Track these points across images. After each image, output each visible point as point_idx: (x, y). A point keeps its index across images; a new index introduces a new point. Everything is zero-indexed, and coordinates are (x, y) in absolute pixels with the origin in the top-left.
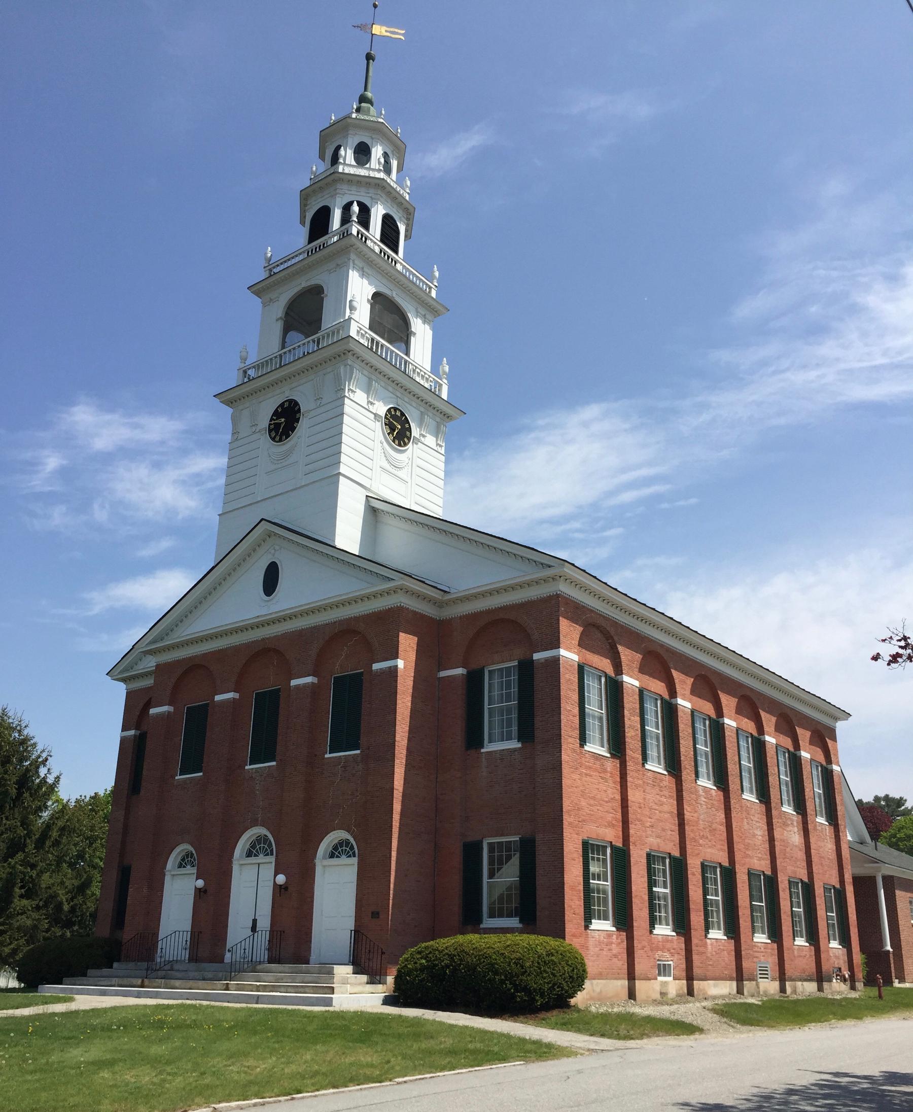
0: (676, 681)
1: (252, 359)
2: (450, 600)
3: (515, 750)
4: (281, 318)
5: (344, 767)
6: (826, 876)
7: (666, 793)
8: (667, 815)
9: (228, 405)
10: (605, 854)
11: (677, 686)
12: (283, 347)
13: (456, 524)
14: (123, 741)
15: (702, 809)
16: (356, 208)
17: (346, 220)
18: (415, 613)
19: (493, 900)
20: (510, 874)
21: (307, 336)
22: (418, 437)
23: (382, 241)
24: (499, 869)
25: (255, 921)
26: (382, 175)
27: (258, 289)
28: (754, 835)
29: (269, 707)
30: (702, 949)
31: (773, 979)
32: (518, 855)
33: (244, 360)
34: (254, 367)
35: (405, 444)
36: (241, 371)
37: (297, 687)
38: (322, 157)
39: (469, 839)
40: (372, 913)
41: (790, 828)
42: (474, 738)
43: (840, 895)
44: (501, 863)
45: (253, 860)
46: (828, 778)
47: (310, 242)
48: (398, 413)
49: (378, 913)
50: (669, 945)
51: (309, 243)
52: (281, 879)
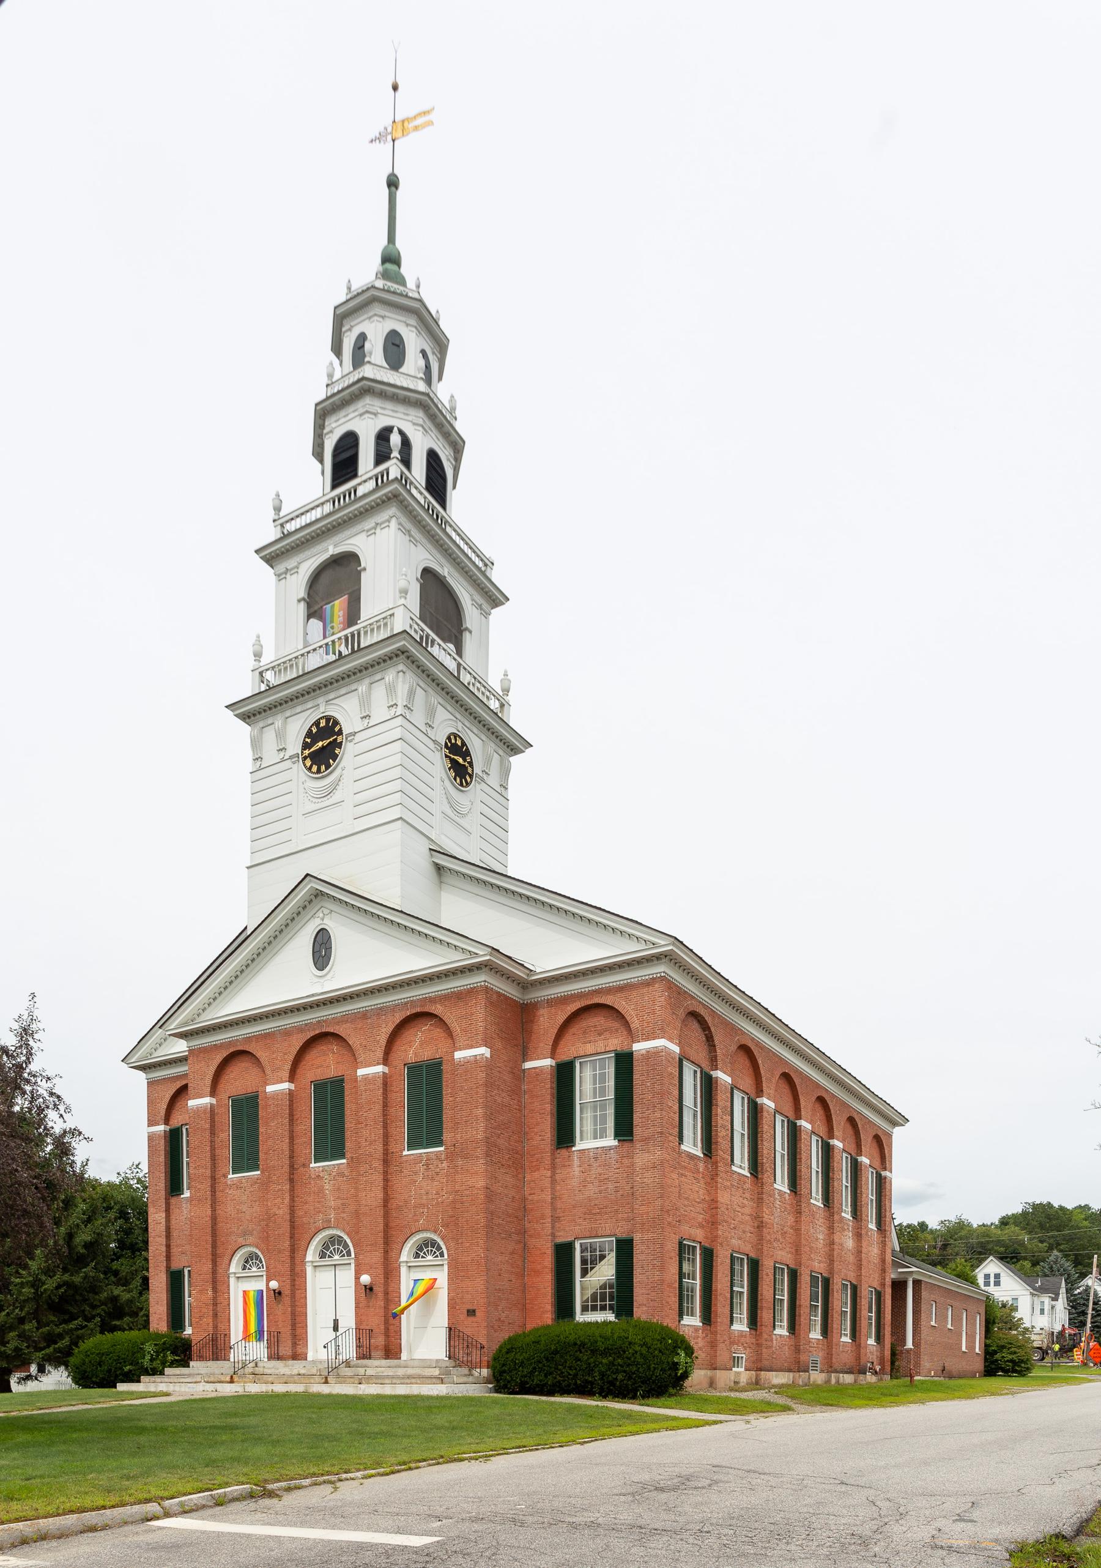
0: (764, 1079)
1: (268, 658)
2: (536, 981)
3: (610, 1148)
4: (303, 599)
5: (427, 1165)
6: (870, 1281)
7: (747, 1195)
8: (748, 1218)
9: (244, 720)
10: (694, 1254)
11: (764, 1085)
12: (325, 637)
13: (543, 889)
14: (151, 1138)
15: (777, 1212)
16: (395, 439)
17: (381, 457)
18: (499, 994)
19: (585, 1298)
20: (606, 1271)
21: (420, 619)
22: (480, 774)
23: (427, 489)
24: (592, 1268)
25: (336, 1322)
26: (422, 387)
27: (272, 556)
28: (817, 1239)
29: (331, 1097)
30: (769, 1343)
31: (822, 1371)
32: (614, 1254)
33: (258, 655)
34: (273, 668)
35: (468, 784)
36: (257, 672)
37: (366, 1078)
38: (337, 349)
39: (559, 1240)
40: (468, 1311)
41: (846, 1233)
42: (565, 1135)
43: (879, 1295)
44: (594, 1262)
45: (327, 1261)
46: (882, 1184)
47: (334, 486)
48: (459, 743)
49: (474, 1311)
50: (743, 1340)
51: (334, 486)
52: (365, 1279)
